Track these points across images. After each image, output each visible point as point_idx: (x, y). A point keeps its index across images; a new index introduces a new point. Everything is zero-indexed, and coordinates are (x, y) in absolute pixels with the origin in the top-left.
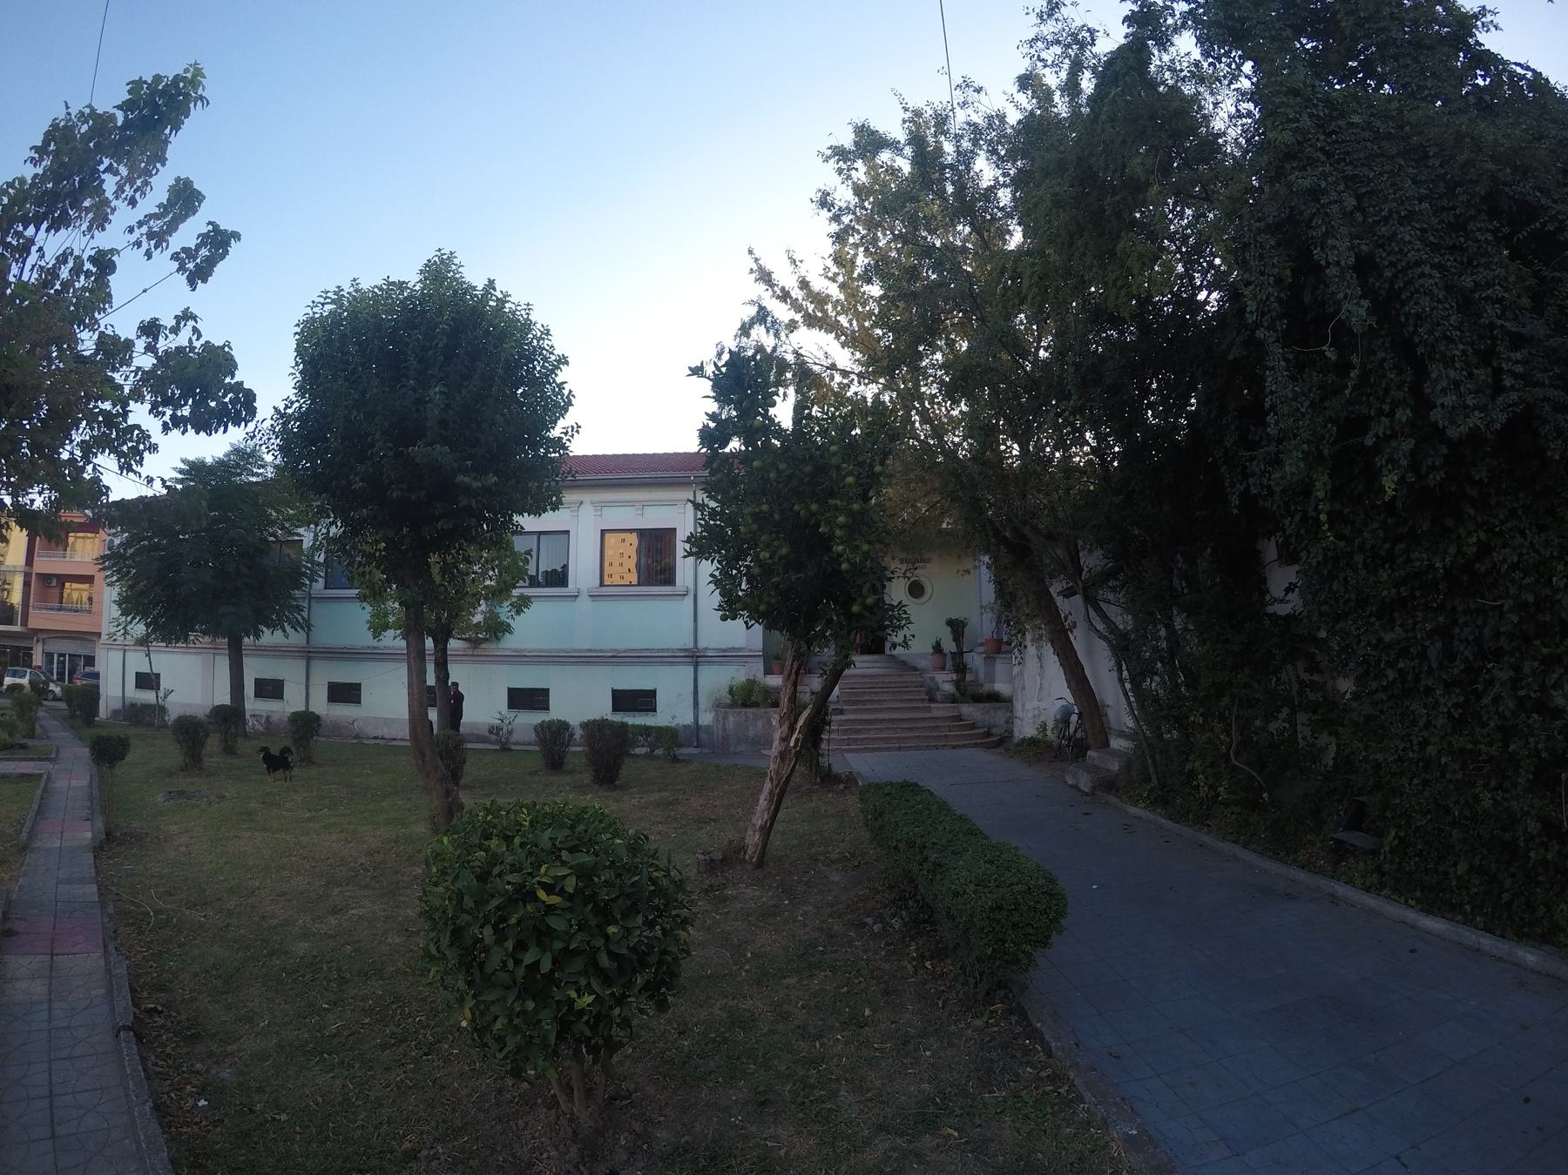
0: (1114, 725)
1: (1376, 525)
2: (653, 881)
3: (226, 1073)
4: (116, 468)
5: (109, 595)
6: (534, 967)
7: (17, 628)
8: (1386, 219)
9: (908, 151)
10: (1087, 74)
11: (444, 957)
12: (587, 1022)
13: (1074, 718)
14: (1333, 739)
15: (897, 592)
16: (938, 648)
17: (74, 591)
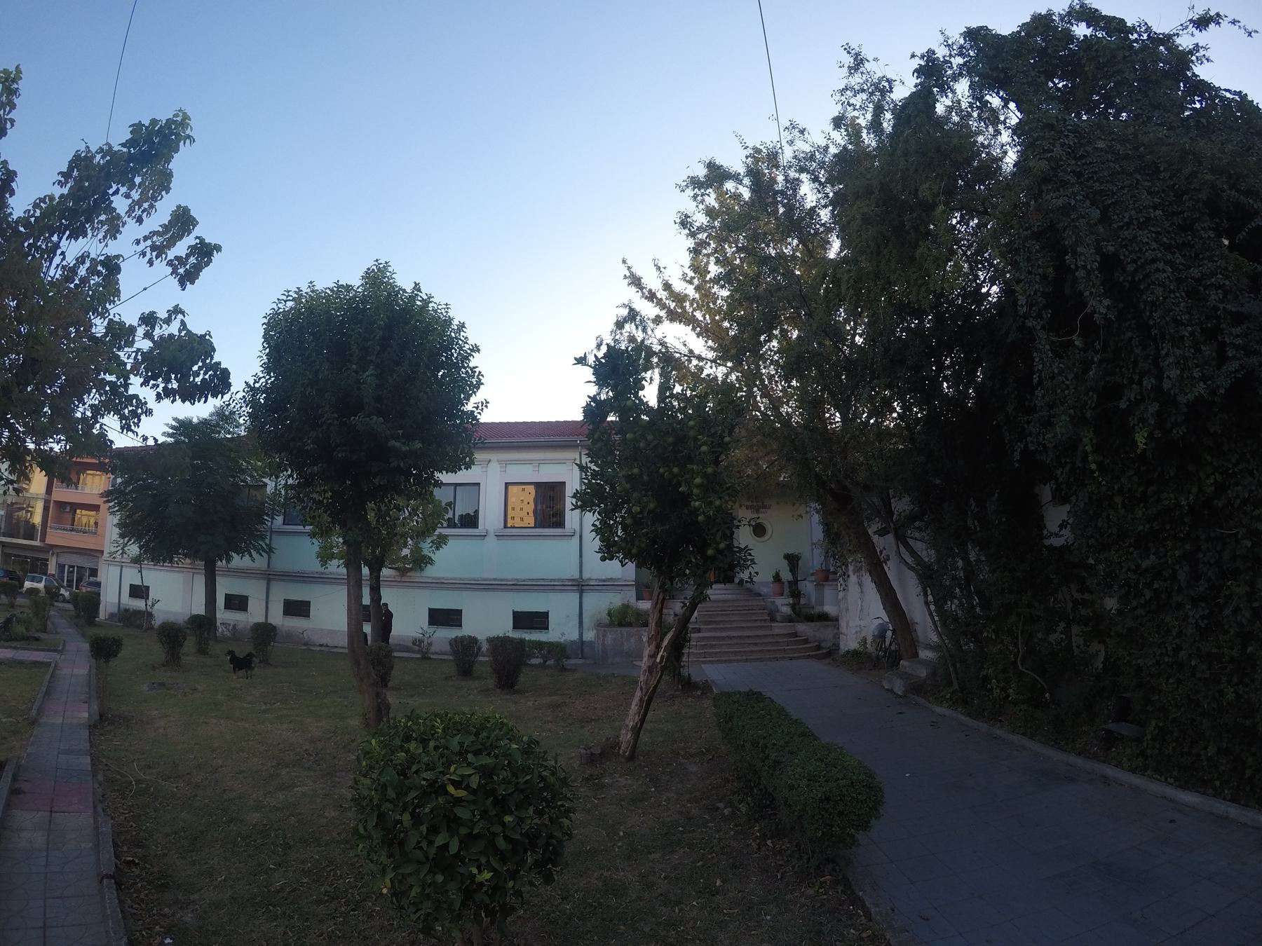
0: (922, 639)
1: (1131, 472)
2: (543, 779)
3: (189, 918)
4: (119, 428)
5: (110, 524)
6: (445, 847)
7: (37, 543)
8: (1128, 225)
9: (747, 181)
10: (888, 115)
11: (370, 837)
12: (486, 892)
13: (889, 634)
14: (1102, 647)
15: (744, 537)
16: (777, 578)
17: (83, 516)
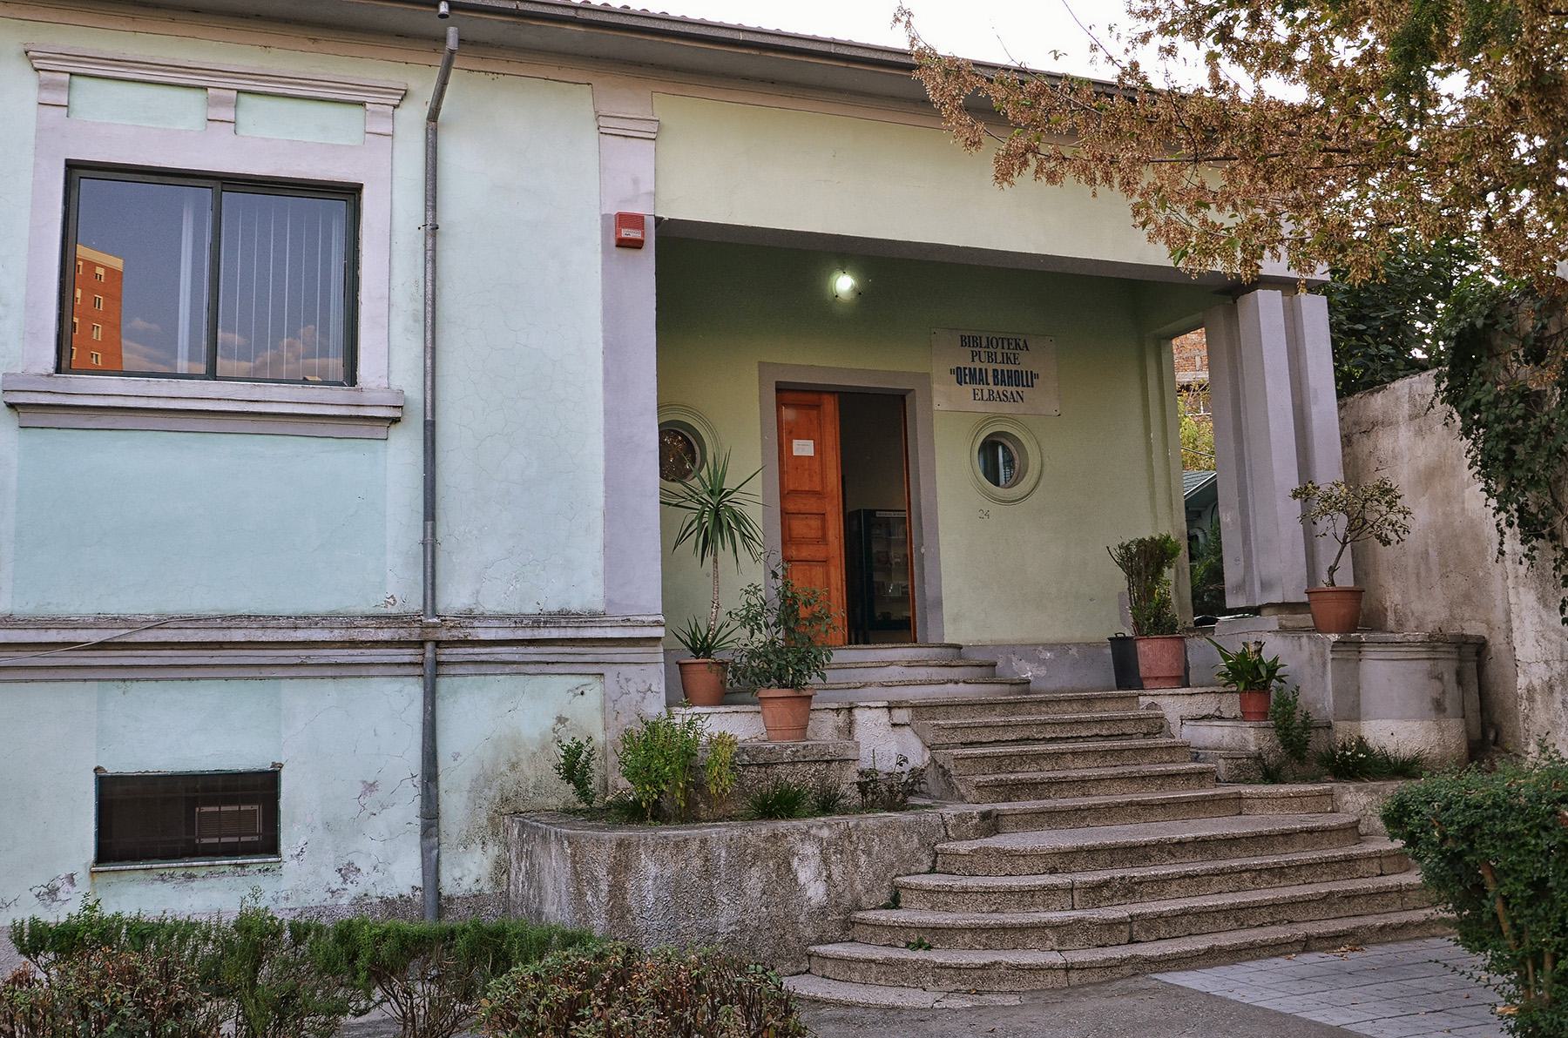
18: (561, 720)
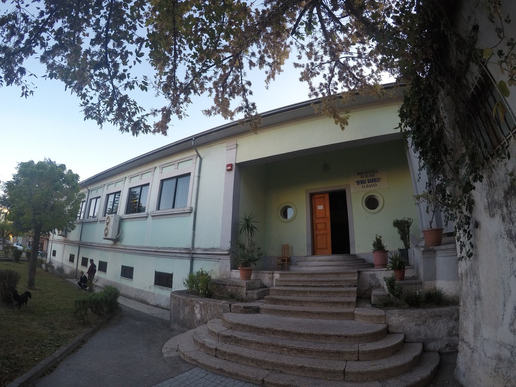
16: (379, 246)
18: (212, 270)
